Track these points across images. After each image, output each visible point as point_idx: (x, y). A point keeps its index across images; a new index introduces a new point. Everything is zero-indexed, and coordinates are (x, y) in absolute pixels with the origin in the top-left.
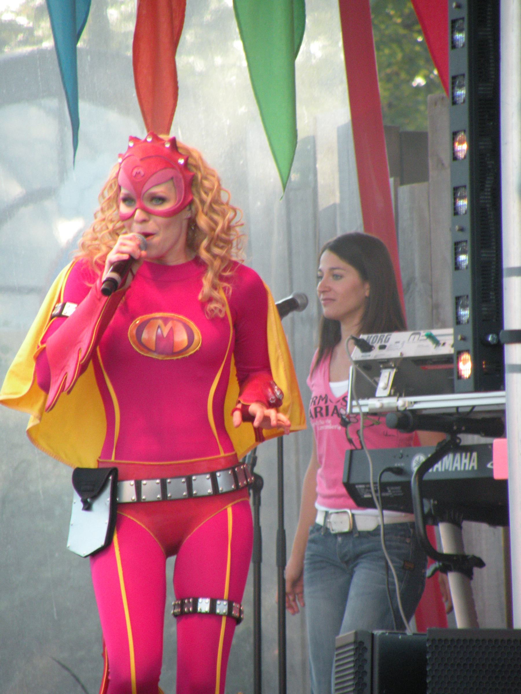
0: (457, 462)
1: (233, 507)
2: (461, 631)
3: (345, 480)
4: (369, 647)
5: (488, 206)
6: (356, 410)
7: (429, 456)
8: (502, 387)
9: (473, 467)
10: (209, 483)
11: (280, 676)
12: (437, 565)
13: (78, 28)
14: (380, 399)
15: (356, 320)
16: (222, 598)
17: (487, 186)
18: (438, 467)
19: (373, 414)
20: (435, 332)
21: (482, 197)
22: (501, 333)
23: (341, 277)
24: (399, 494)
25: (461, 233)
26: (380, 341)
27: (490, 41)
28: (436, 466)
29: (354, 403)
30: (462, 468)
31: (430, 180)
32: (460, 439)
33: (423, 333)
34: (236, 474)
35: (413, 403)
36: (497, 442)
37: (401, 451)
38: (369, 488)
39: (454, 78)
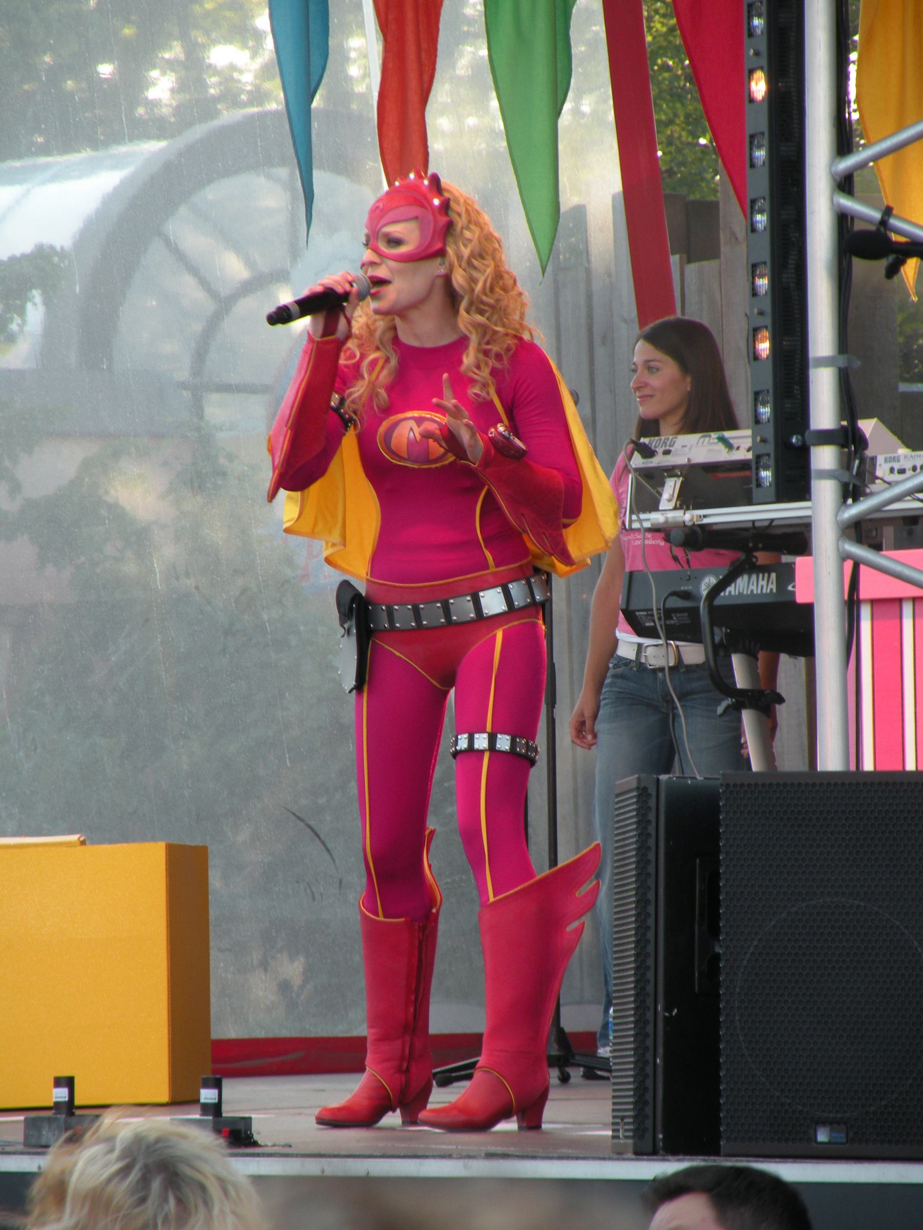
0: (753, 584)
3: (624, 607)
4: (654, 794)
5: (792, 285)
6: (636, 525)
7: (721, 577)
8: (807, 497)
9: (771, 590)
11: (550, 826)
12: (728, 701)
14: (663, 512)
15: (675, 418)
16: (484, 731)
17: (790, 262)
18: (731, 590)
19: (655, 530)
20: (727, 434)
21: (785, 275)
22: (807, 433)
23: (658, 369)
24: (686, 622)
26: (664, 445)
28: (728, 589)
29: (634, 517)
30: (759, 592)
31: (722, 256)
33: (714, 435)
34: (415, 617)
35: (702, 517)
36: (799, 560)
38: (652, 615)
39: (752, 137)
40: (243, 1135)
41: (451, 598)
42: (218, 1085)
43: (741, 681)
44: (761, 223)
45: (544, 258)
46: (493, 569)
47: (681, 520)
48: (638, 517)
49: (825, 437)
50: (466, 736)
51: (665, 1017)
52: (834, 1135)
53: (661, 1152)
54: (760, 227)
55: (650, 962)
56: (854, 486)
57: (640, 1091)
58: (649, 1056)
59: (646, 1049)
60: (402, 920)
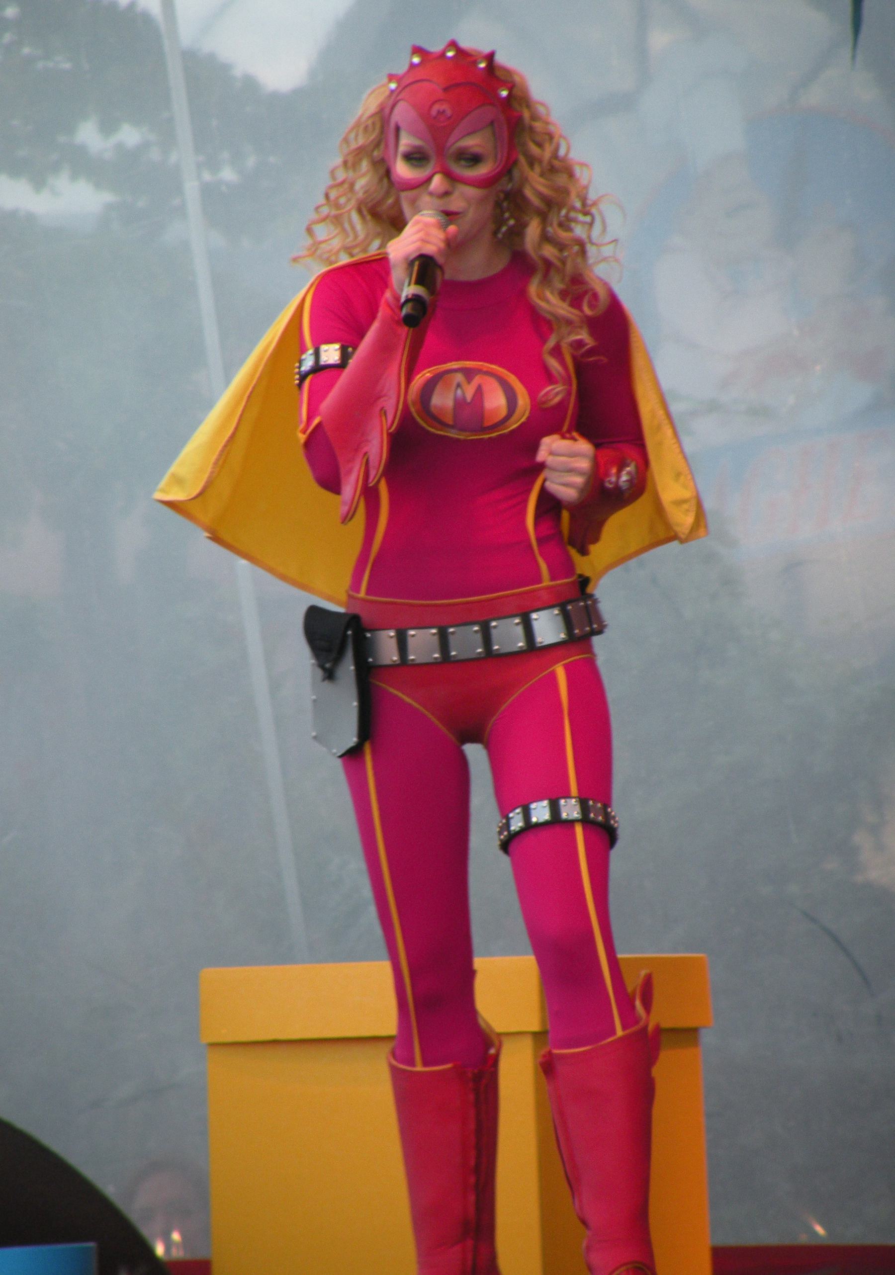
1: (567, 668)
10: (520, 631)
16: (567, 796)
41: (494, 619)
46: (546, 582)
50: (545, 803)
60: (448, 1066)
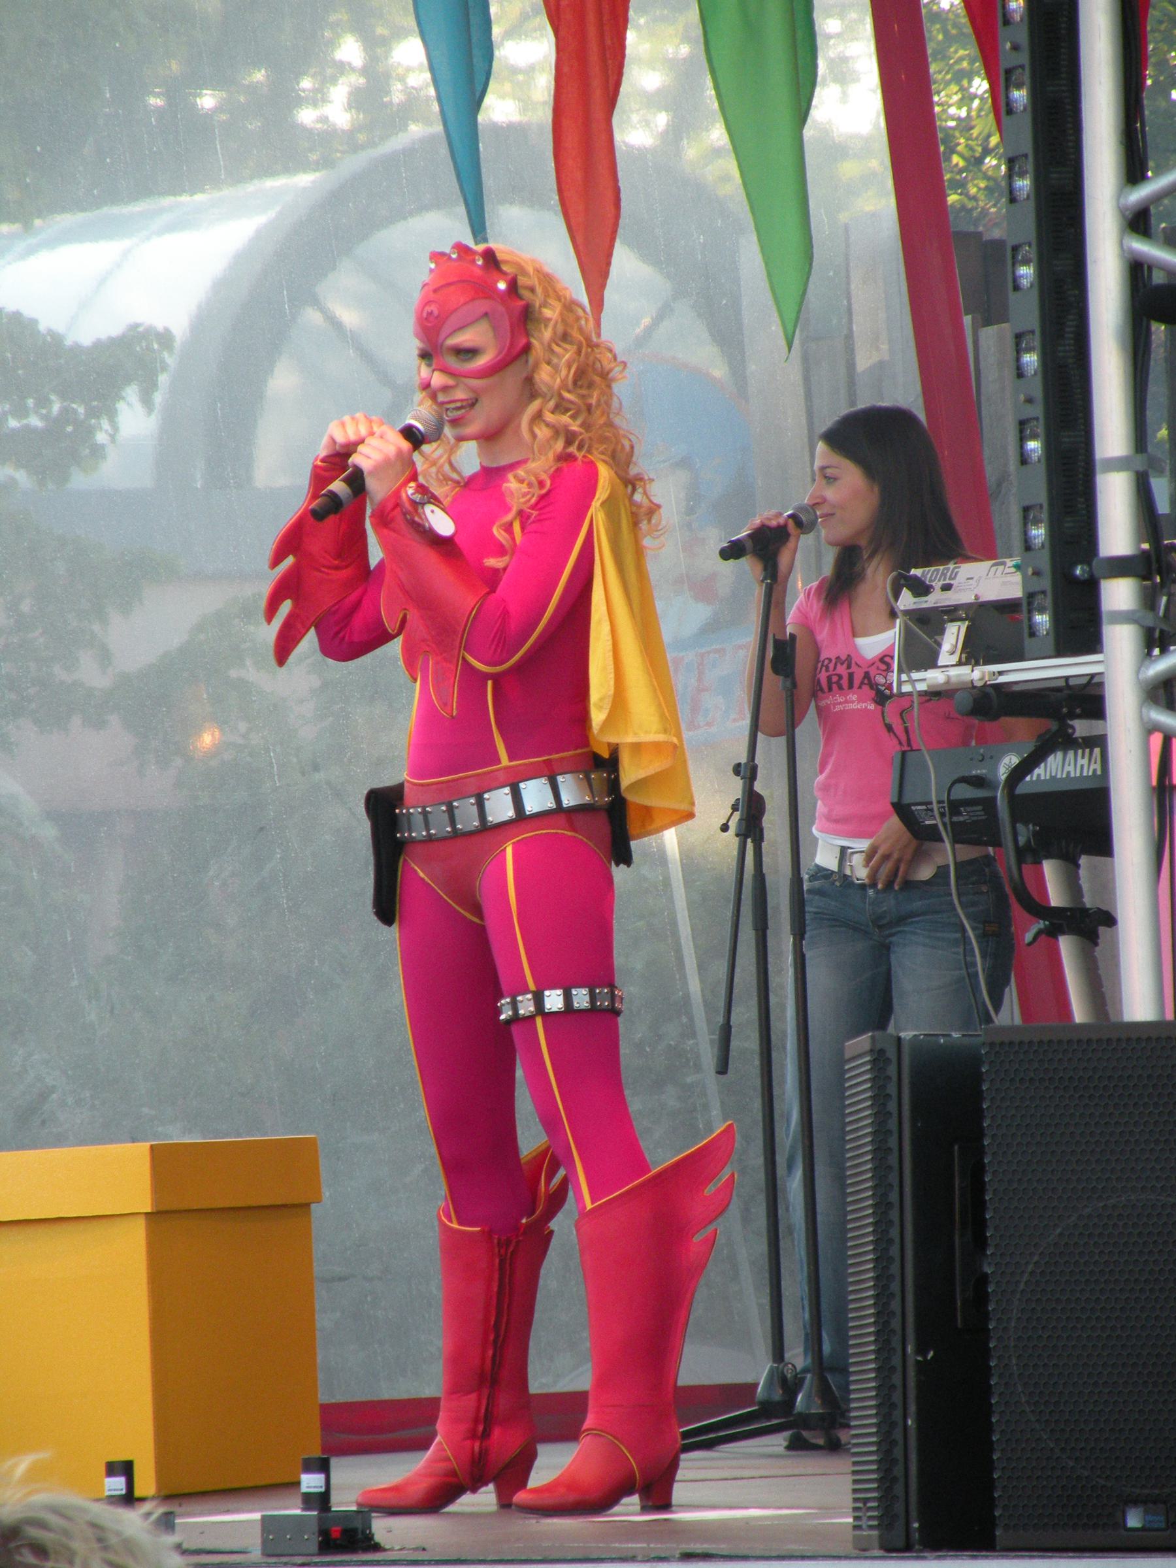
2: (1082, 1026)
3: (895, 800)
4: (894, 1058)
5: (1070, 361)
6: (906, 688)
9: (1095, 771)
12: (1041, 924)
13: (479, 88)
18: (1039, 771)
19: (934, 695)
21: (1060, 348)
22: (1094, 563)
23: (835, 479)
25: (1028, 406)
27: (1067, 101)
28: (1037, 771)
29: (904, 677)
30: (1078, 775)
32: (1073, 727)
35: (997, 674)
37: (982, 751)
38: (932, 810)
40: (360, 1536)
42: (323, 1467)
43: (1056, 897)
44: (1026, 278)
45: (790, 327)
46: (505, 760)
47: (968, 679)
48: (909, 677)
49: (1120, 567)
51: (918, 1362)
52: (1150, 1518)
53: (917, 1547)
54: (1025, 283)
55: (895, 1287)
56: (1162, 632)
57: (887, 1463)
58: (897, 1414)
59: (893, 1406)
